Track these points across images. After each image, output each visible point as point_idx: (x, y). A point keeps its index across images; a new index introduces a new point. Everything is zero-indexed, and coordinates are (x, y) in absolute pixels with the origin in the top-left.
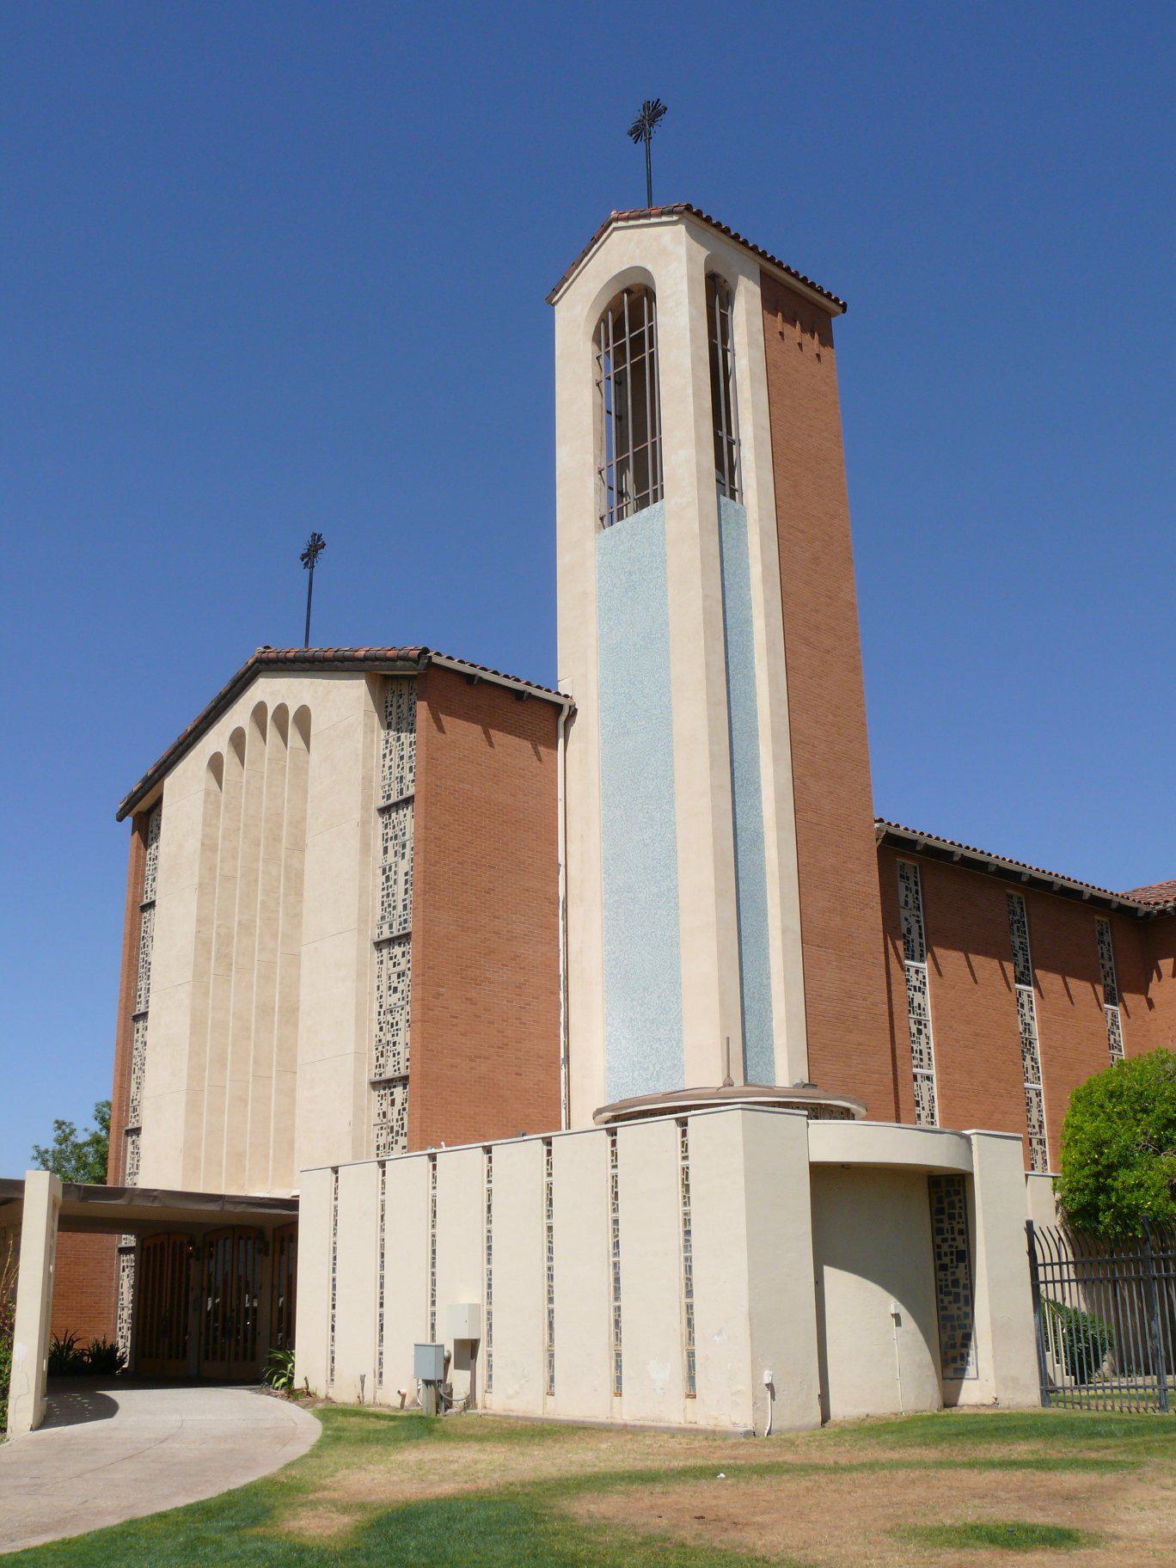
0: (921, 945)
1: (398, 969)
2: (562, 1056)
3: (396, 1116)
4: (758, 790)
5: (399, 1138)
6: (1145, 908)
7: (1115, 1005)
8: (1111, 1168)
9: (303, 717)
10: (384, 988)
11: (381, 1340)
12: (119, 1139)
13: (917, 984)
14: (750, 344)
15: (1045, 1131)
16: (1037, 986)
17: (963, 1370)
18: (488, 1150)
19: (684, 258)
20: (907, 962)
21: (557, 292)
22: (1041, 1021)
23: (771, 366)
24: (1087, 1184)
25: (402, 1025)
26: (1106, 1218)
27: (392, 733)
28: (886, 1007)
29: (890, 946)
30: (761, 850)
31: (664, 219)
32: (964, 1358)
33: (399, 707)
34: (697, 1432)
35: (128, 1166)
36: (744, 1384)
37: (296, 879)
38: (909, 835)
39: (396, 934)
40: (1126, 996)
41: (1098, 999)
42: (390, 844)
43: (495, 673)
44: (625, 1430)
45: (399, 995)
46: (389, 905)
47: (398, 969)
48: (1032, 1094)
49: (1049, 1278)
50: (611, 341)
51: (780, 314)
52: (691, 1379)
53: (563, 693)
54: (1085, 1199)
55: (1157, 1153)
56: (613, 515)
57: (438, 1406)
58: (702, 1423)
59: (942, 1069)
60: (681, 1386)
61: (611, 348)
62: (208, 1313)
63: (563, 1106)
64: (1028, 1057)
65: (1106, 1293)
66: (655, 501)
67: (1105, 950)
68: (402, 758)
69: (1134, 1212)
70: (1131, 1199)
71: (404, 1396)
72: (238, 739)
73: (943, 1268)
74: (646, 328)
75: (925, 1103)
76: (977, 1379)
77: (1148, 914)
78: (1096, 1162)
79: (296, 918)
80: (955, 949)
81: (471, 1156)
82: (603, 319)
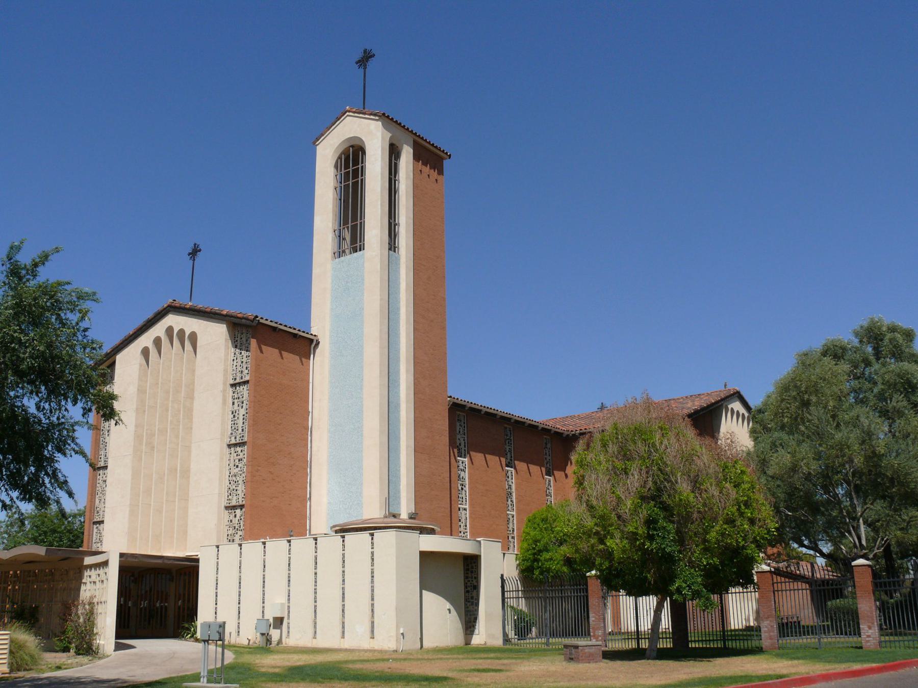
0: (465, 450)
1: (238, 457)
2: (308, 496)
3: (237, 522)
4: (399, 385)
5: (238, 532)
6: (566, 433)
7: (550, 476)
8: (540, 551)
9: (193, 337)
10: (232, 465)
11: (239, 618)
12: (90, 526)
13: (462, 468)
14: (407, 178)
15: (515, 532)
16: (515, 469)
17: (473, 631)
18: (289, 541)
19: (380, 138)
20: (459, 458)
21: (318, 140)
22: (516, 484)
23: (416, 187)
24: (530, 558)
25: (240, 482)
26: (537, 572)
27: (237, 350)
28: (449, 479)
29: (451, 451)
30: (399, 412)
31: (372, 117)
32: (474, 626)
33: (241, 339)
34: (375, 651)
35: (94, 539)
36: (393, 633)
37: (189, 412)
38: (463, 403)
39: (238, 442)
40: (555, 472)
41: (542, 474)
42: (236, 401)
43: (285, 326)
44: (346, 650)
45: (239, 469)
46: (235, 429)
47: (238, 457)
48: (510, 517)
49: (509, 596)
50: (359, 224)
51: (421, 162)
52: (372, 632)
53: (314, 334)
54: (529, 564)
55: (559, 546)
56: (340, 253)
57: (267, 643)
58: (376, 648)
59: (471, 505)
60: (368, 634)
61: (343, 172)
62: (141, 609)
63: (308, 519)
64: (509, 500)
65: (533, 603)
66: (360, 250)
67: (547, 452)
68: (242, 362)
69: (548, 570)
70: (547, 565)
71: (249, 640)
72: (157, 342)
73: (468, 592)
74: (360, 166)
75: (463, 520)
76: (479, 634)
77: (568, 435)
78: (534, 549)
79: (189, 429)
80: (480, 452)
81: (282, 543)
82: (340, 158)
